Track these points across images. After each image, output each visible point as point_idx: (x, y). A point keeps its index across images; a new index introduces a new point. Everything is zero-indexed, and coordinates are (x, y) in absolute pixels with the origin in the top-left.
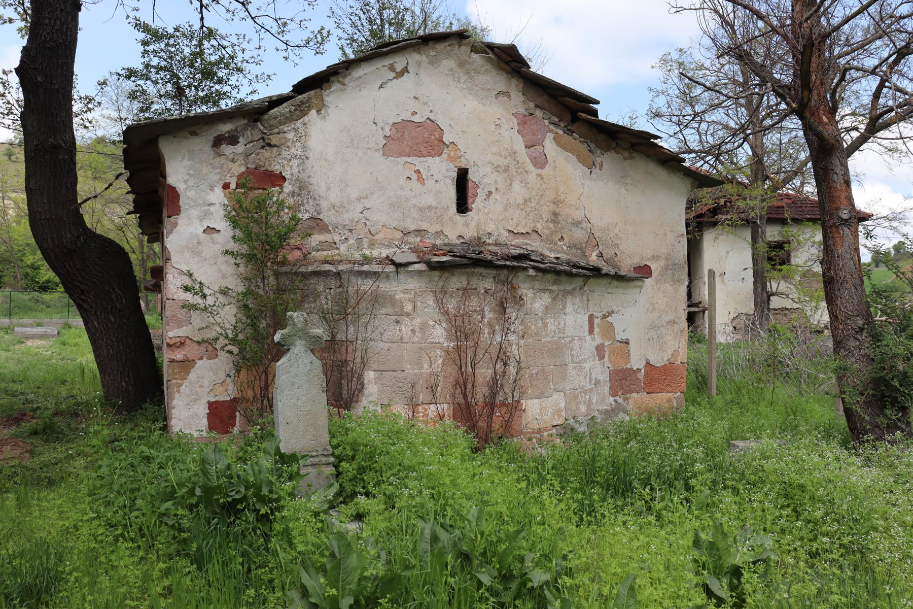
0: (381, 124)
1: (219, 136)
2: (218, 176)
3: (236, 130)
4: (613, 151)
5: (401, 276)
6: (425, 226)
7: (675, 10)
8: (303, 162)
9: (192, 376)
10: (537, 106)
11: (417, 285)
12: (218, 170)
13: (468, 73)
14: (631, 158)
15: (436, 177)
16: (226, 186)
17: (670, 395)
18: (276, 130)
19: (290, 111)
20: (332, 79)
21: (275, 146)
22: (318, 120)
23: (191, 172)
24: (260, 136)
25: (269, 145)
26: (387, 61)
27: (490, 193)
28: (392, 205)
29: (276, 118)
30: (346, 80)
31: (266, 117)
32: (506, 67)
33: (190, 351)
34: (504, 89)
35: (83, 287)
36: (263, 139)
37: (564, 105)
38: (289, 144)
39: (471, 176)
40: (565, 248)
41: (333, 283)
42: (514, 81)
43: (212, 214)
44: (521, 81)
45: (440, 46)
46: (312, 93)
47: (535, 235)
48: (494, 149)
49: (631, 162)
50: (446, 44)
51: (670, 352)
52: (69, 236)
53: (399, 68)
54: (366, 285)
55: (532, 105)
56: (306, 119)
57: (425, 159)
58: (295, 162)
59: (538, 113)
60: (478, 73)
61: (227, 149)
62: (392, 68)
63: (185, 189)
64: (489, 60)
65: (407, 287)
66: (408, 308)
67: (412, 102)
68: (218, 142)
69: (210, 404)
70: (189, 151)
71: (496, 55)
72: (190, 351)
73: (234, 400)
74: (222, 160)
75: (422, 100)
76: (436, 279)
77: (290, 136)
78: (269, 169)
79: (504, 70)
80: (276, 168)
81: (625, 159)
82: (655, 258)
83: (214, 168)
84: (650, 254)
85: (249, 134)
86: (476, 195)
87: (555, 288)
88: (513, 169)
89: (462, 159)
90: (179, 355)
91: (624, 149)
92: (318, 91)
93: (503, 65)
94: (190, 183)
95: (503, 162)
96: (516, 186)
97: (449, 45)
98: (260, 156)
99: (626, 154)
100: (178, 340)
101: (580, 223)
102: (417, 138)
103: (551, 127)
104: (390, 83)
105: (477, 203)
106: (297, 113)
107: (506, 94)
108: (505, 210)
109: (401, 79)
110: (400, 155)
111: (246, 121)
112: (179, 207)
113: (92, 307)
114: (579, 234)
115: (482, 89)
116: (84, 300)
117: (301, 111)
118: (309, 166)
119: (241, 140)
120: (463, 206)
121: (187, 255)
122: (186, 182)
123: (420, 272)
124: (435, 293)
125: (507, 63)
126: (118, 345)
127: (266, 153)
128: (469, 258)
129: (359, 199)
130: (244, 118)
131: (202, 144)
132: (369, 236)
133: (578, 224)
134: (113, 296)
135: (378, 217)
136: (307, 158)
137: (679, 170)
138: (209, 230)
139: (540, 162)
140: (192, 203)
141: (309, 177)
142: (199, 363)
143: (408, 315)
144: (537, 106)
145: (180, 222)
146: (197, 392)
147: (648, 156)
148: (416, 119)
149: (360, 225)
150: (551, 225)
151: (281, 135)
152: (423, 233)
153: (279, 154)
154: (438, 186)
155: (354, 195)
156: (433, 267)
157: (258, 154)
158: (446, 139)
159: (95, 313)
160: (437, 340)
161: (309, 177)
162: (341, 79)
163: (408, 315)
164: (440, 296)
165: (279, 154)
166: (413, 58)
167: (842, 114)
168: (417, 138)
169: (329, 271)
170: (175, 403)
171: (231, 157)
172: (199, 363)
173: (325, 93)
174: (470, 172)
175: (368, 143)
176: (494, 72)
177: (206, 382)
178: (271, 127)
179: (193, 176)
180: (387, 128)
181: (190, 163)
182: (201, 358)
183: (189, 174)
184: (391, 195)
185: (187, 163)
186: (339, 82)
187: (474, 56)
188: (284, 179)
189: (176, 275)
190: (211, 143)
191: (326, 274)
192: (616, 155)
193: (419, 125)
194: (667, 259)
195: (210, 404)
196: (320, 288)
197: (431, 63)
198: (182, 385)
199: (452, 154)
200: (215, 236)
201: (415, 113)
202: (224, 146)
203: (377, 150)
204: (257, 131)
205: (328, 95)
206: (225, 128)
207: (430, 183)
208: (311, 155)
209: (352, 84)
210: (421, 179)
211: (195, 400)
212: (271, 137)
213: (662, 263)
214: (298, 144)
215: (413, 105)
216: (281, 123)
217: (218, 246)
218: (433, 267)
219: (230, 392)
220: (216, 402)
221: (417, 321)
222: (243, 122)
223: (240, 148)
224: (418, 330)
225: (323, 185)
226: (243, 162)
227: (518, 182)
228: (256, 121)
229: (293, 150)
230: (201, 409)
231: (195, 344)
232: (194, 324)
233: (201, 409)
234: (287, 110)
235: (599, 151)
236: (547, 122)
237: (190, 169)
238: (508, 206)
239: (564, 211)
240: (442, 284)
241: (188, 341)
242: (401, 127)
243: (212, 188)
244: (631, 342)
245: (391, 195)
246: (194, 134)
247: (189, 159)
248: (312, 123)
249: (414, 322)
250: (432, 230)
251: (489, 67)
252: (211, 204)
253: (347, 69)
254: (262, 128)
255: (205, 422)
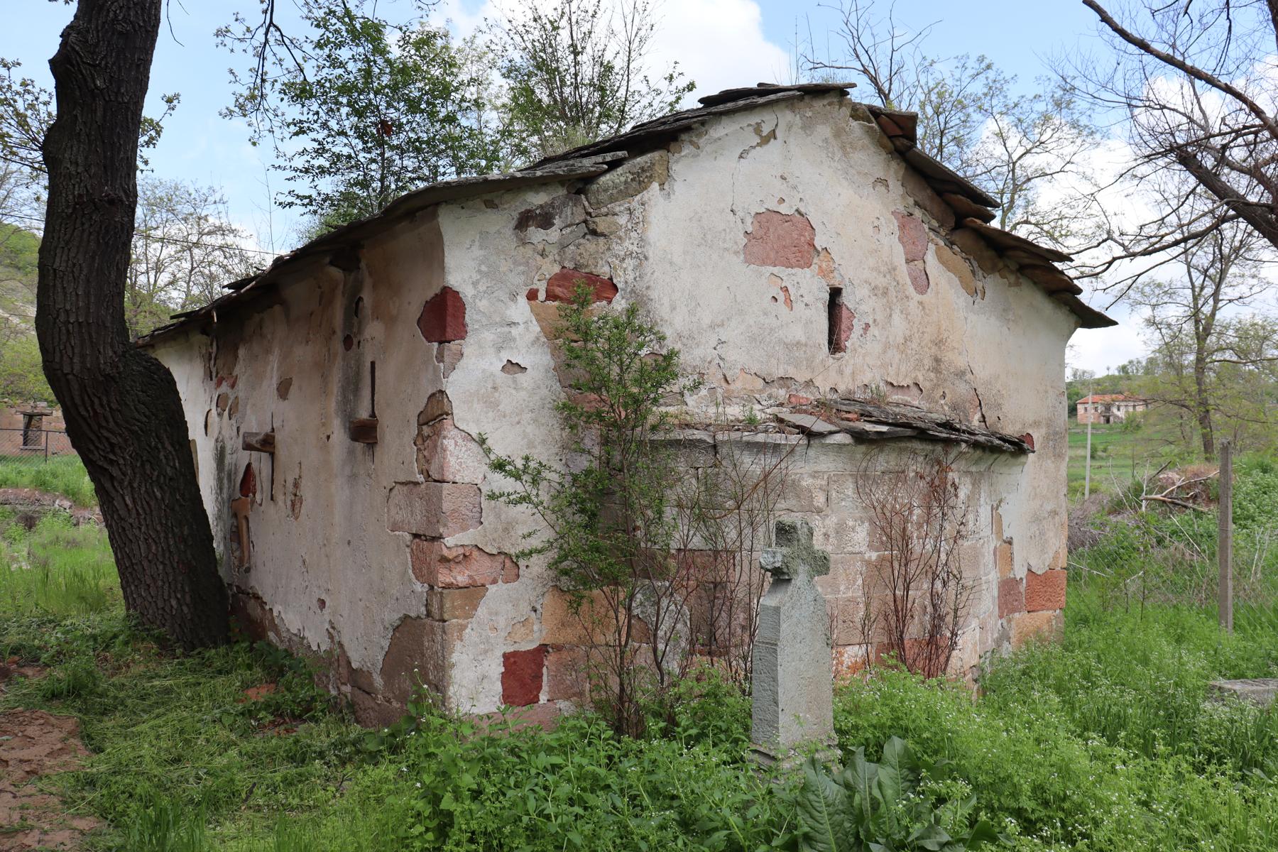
0: (740, 214)
1: (529, 211)
2: (523, 278)
3: (552, 205)
4: (997, 275)
5: (811, 452)
6: (791, 372)
7: (811, 66)
8: (641, 264)
9: (482, 611)
10: (916, 204)
11: (832, 466)
12: (522, 268)
13: (843, 148)
14: (1017, 284)
15: (806, 299)
16: (532, 296)
17: (1050, 612)
18: (604, 210)
19: (626, 182)
20: (684, 137)
21: (603, 235)
22: (661, 200)
23: (484, 268)
24: (582, 218)
25: (594, 233)
26: (754, 119)
27: (867, 325)
28: (753, 339)
29: (606, 190)
30: (702, 142)
31: (595, 187)
32: (890, 144)
33: (481, 569)
34: (881, 175)
35: (114, 440)
36: (585, 221)
37: (948, 204)
38: (621, 234)
39: (847, 299)
40: (946, 408)
41: (703, 459)
42: (894, 165)
43: (514, 340)
44: (903, 165)
45: (819, 104)
46: (656, 155)
47: (914, 390)
48: (872, 262)
49: (1016, 289)
50: (825, 102)
51: (1051, 555)
52: (111, 353)
53: (766, 130)
54: (752, 465)
55: (911, 201)
56: (645, 195)
57: (794, 271)
58: (630, 263)
59: (918, 213)
60: (854, 148)
61: (536, 235)
62: (758, 130)
63: (475, 297)
64: (870, 131)
65: (817, 468)
66: (820, 500)
67: (778, 182)
68: (524, 221)
69: (506, 657)
70: (481, 233)
71: (879, 124)
72: (481, 569)
73: (543, 649)
74: (528, 251)
75: (792, 181)
76: (859, 456)
77: (622, 220)
78: (595, 271)
79: (883, 146)
80: (604, 271)
81: (1010, 285)
82: (1036, 424)
83: (516, 263)
84: (1030, 418)
85: (569, 213)
86: (851, 328)
87: (973, 469)
88: (892, 293)
89: (836, 273)
90: (461, 577)
91: (1011, 272)
92: (663, 153)
93: (886, 141)
94: (482, 287)
95: (881, 281)
96: (897, 318)
97: (830, 104)
98: (582, 250)
99: (1012, 278)
100: (461, 551)
101: (963, 373)
102: (783, 239)
103: (931, 234)
104: (753, 153)
105: (852, 341)
106: (634, 184)
107: (883, 182)
108: (885, 352)
109: (766, 147)
110: (764, 263)
111: (565, 192)
112: (464, 325)
113: (124, 474)
114: (962, 389)
115: (859, 173)
116: (111, 462)
117: (640, 182)
118: (648, 270)
119: (557, 221)
120: (835, 344)
121: (477, 406)
122: (475, 284)
123: (841, 446)
124: (856, 478)
125: (890, 137)
126: (166, 538)
127: (590, 245)
128: (916, 428)
129: (712, 327)
130: (563, 185)
131: (500, 222)
132: (724, 385)
133: (960, 374)
134: (162, 457)
135: (737, 356)
136: (646, 258)
137: (1066, 303)
138: (512, 367)
139: (922, 282)
140: (484, 321)
141: (648, 288)
142: (492, 589)
143: (819, 511)
144: (916, 204)
145: (466, 351)
146: (488, 638)
147: (1035, 283)
148: (784, 209)
149: (713, 369)
150: (932, 375)
151: (609, 218)
152: (789, 382)
153: (609, 249)
154: (808, 312)
155: (706, 321)
156: (860, 438)
157: (578, 246)
158: (819, 243)
159: (130, 483)
160: (857, 549)
161: (648, 288)
162: (694, 139)
163: (819, 511)
164: (863, 479)
165: (609, 249)
166: (785, 118)
167: (1015, 221)
168: (783, 239)
169: (701, 441)
170: (455, 658)
171: (540, 247)
172: (492, 589)
173: (673, 158)
174: (844, 293)
175: (724, 241)
176: (872, 149)
177: (501, 622)
178: (599, 204)
179: (486, 275)
180: (749, 220)
181: (482, 252)
182: (494, 582)
183: (479, 271)
184: (752, 323)
185: (477, 252)
186: (691, 142)
187: (854, 124)
188: (615, 289)
189: (460, 441)
190: (514, 223)
191: (693, 444)
192: (1001, 280)
193: (787, 218)
194: (1048, 426)
195: (506, 657)
196: (682, 467)
197: (804, 128)
198: (466, 627)
199: (824, 265)
200: (520, 376)
201: (782, 200)
202: (532, 229)
203: (736, 253)
204: (580, 210)
205: (677, 162)
206: (537, 199)
207: (799, 306)
208: (650, 254)
209: (708, 148)
210: (789, 302)
211: (486, 652)
212: (597, 219)
213: (1043, 431)
214: (633, 234)
215: (780, 189)
216: (613, 199)
217: (523, 394)
218: (860, 438)
219: (536, 635)
220: (515, 654)
221: (832, 521)
222: (561, 192)
223: (553, 234)
224: (832, 534)
225: (666, 301)
226: (557, 258)
227: (898, 311)
228: (579, 192)
229: (627, 243)
230: (493, 666)
231: (486, 557)
232: (486, 523)
233: (493, 666)
234: (623, 179)
235: (980, 273)
236: (926, 226)
237: (482, 262)
238: (887, 347)
239: (948, 356)
240: (864, 464)
241: (476, 553)
242: (767, 219)
243: (514, 297)
244: (1015, 541)
245: (752, 323)
246: (491, 205)
247: (481, 247)
248: (652, 203)
249: (827, 522)
250: (802, 377)
251: (866, 141)
252: (512, 324)
253: (703, 124)
254: (586, 204)
255: (498, 687)
